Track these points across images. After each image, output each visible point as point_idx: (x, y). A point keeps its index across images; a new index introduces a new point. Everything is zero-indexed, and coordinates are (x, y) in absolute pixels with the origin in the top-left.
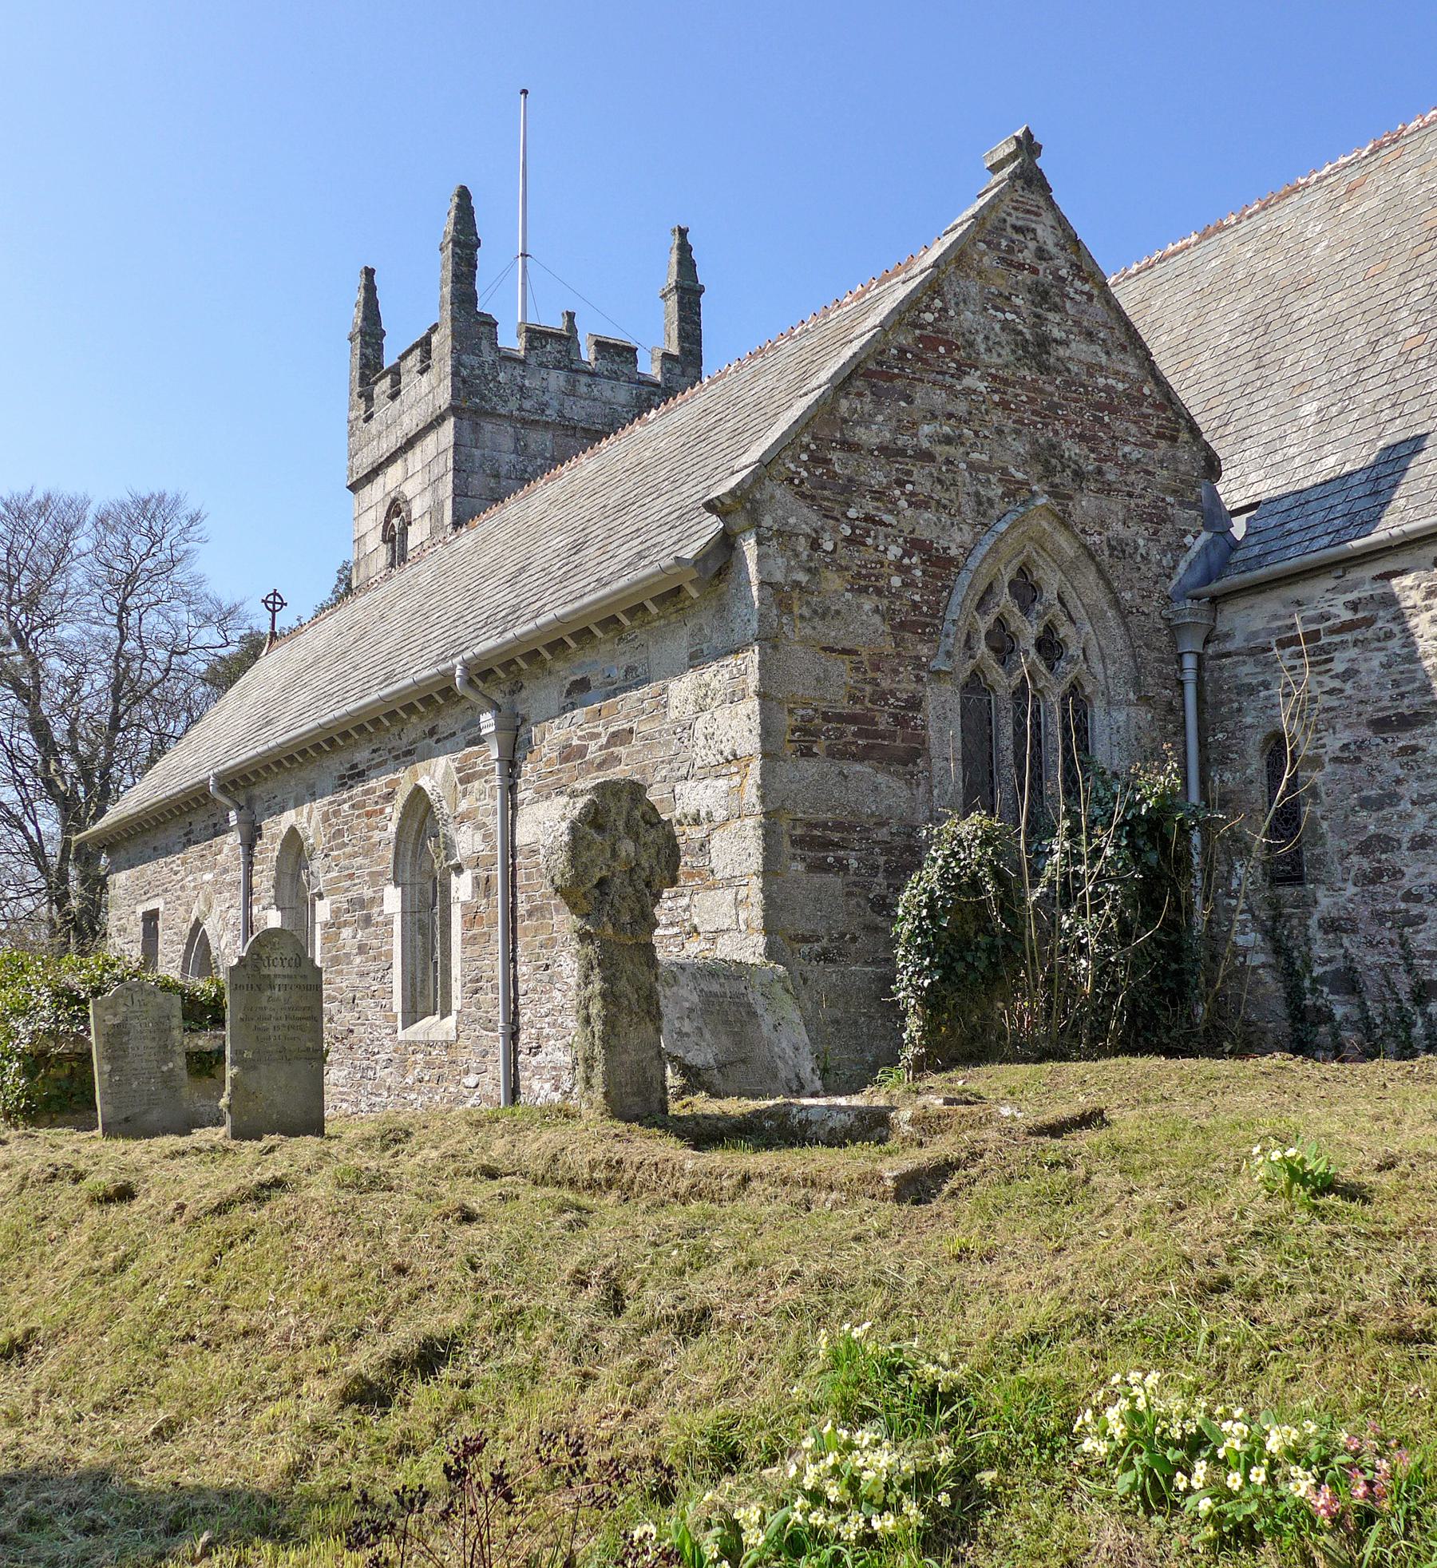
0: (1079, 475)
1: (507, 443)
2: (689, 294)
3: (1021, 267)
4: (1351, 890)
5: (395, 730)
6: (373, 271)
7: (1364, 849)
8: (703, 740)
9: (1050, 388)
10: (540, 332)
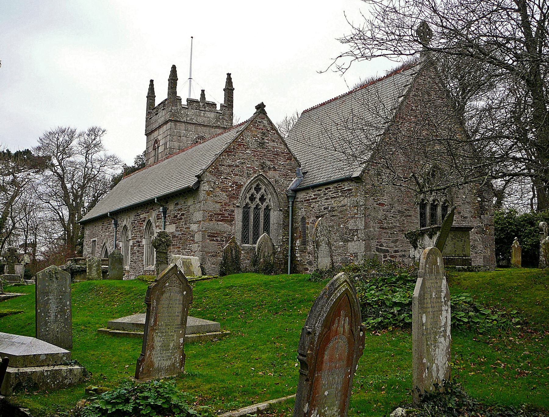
0: (270, 168)
2: (229, 90)
3: (260, 129)
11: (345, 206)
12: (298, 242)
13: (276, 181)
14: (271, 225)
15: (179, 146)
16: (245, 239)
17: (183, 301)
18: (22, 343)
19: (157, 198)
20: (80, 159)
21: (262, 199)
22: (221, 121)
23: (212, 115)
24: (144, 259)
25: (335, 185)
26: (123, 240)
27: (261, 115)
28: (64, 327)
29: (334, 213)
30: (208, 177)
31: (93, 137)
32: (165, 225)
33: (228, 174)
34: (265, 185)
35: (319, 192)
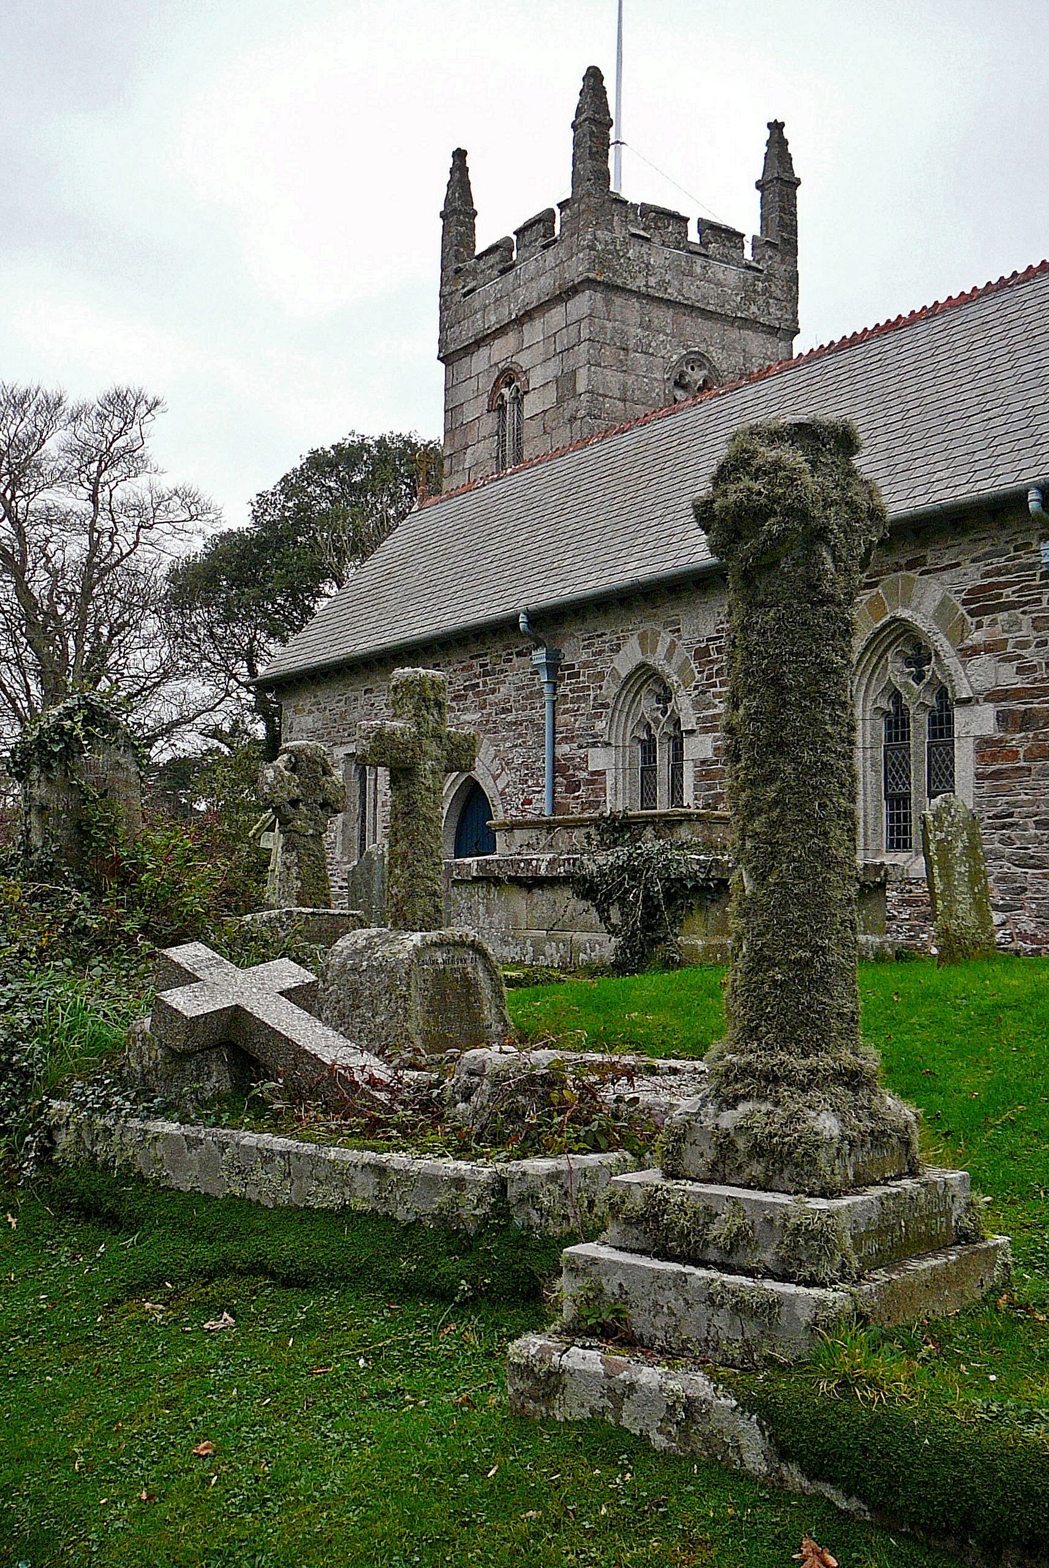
1: (634, 317)
2: (779, 183)
6: (783, 125)
10: (662, 213)
15: (624, 388)
19: (528, 613)
20: (72, 500)
22: (761, 300)
23: (731, 275)
31: (117, 423)
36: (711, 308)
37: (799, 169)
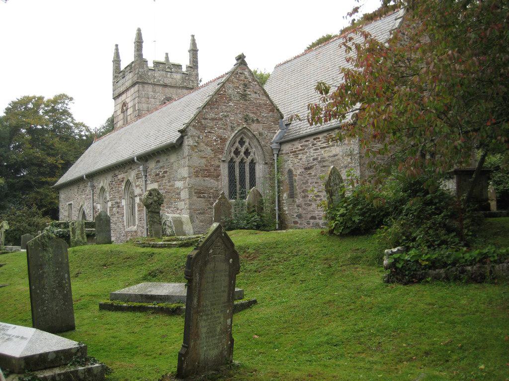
0: (253, 121)
2: (194, 51)
4: (301, 199)
5: (123, 167)
7: (303, 192)
8: (181, 175)
9: (247, 104)
11: (336, 155)
12: (285, 195)
13: (260, 134)
14: (257, 179)
16: (232, 193)
17: (230, 272)
18: (22, 338)
21: (247, 153)
24: (125, 220)
25: (325, 134)
26: (101, 201)
27: (243, 66)
28: (64, 304)
29: (324, 164)
30: (192, 131)
32: (146, 184)
33: (212, 128)
34: (250, 138)
35: (307, 143)
36: (173, 85)
37: (198, 47)
